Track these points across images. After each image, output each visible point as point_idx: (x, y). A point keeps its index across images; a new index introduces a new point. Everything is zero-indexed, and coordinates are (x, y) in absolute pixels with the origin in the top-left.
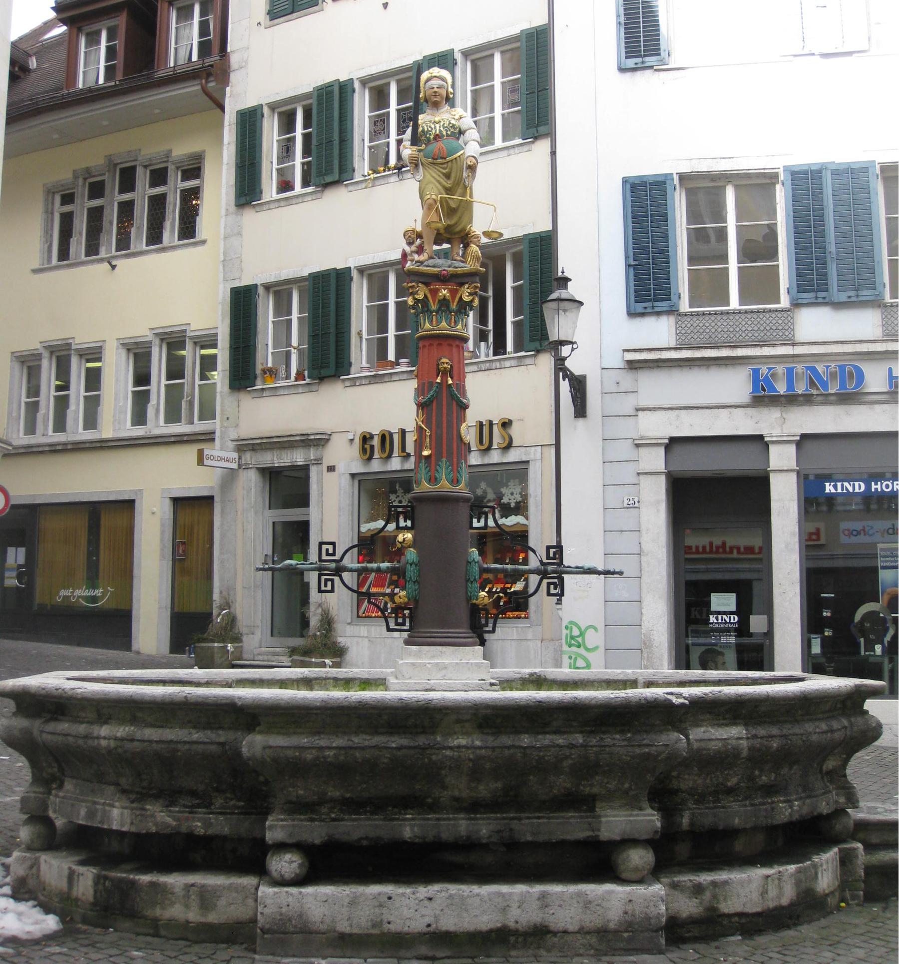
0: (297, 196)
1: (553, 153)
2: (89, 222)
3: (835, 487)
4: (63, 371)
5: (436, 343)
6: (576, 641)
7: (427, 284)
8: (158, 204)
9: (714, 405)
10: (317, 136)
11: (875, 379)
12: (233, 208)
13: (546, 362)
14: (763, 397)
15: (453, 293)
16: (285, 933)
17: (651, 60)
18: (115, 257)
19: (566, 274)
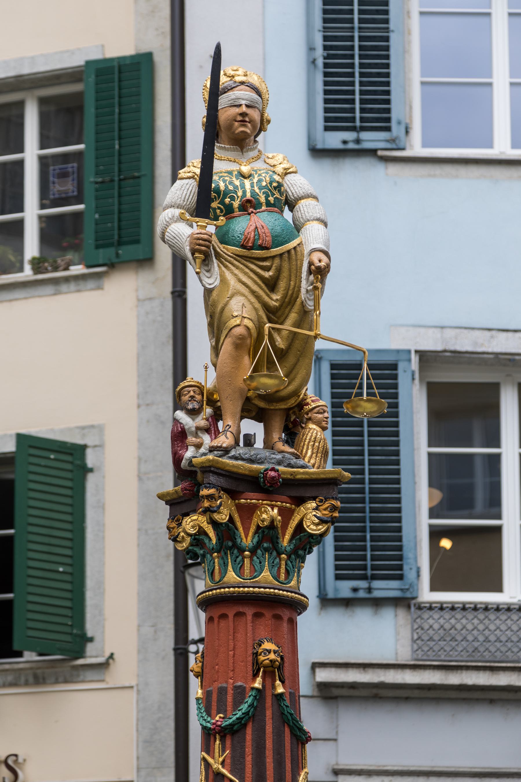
5: (249, 611)
7: (233, 494)
15: (286, 515)
17: (371, 139)
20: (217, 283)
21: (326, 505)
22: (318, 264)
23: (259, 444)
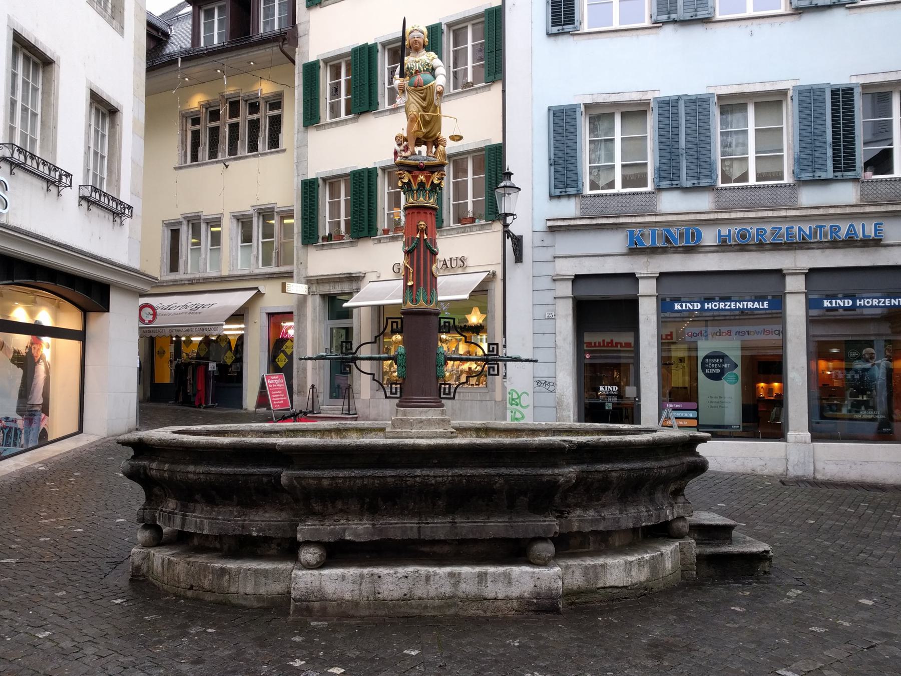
0: (342, 121)
1: (504, 91)
2: (210, 137)
3: (681, 306)
4: (196, 233)
5: (416, 211)
6: (515, 402)
7: (410, 172)
8: (254, 125)
9: (604, 254)
11: (709, 237)
12: (302, 128)
13: (498, 226)
14: (635, 250)
15: (428, 178)
16: (309, 601)
17: (568, 28)
18: (227, 160)
19: (510, 170)
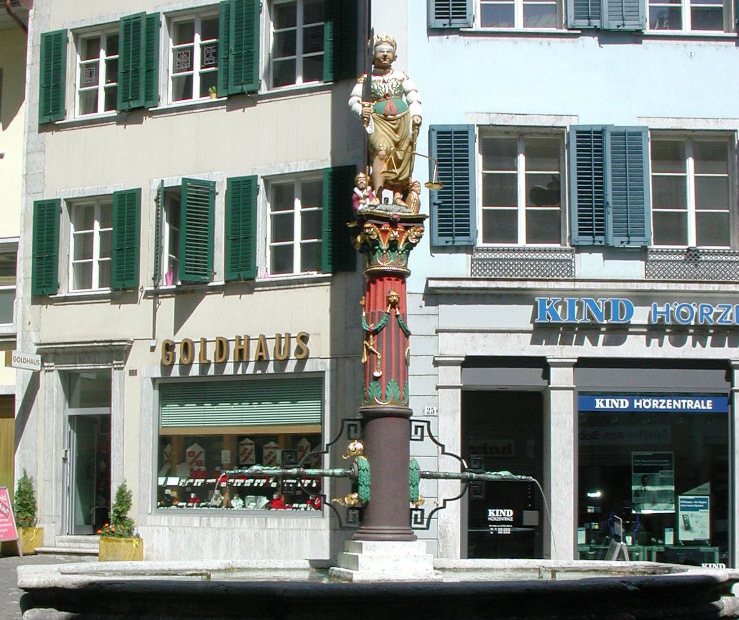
3: (604, 403)
9: (504, 331)
10: (124, 64)
17: (457, 23)
20: (373, 131)
21: (419, 230)
22: (416, 122)
23: (391, 202)
